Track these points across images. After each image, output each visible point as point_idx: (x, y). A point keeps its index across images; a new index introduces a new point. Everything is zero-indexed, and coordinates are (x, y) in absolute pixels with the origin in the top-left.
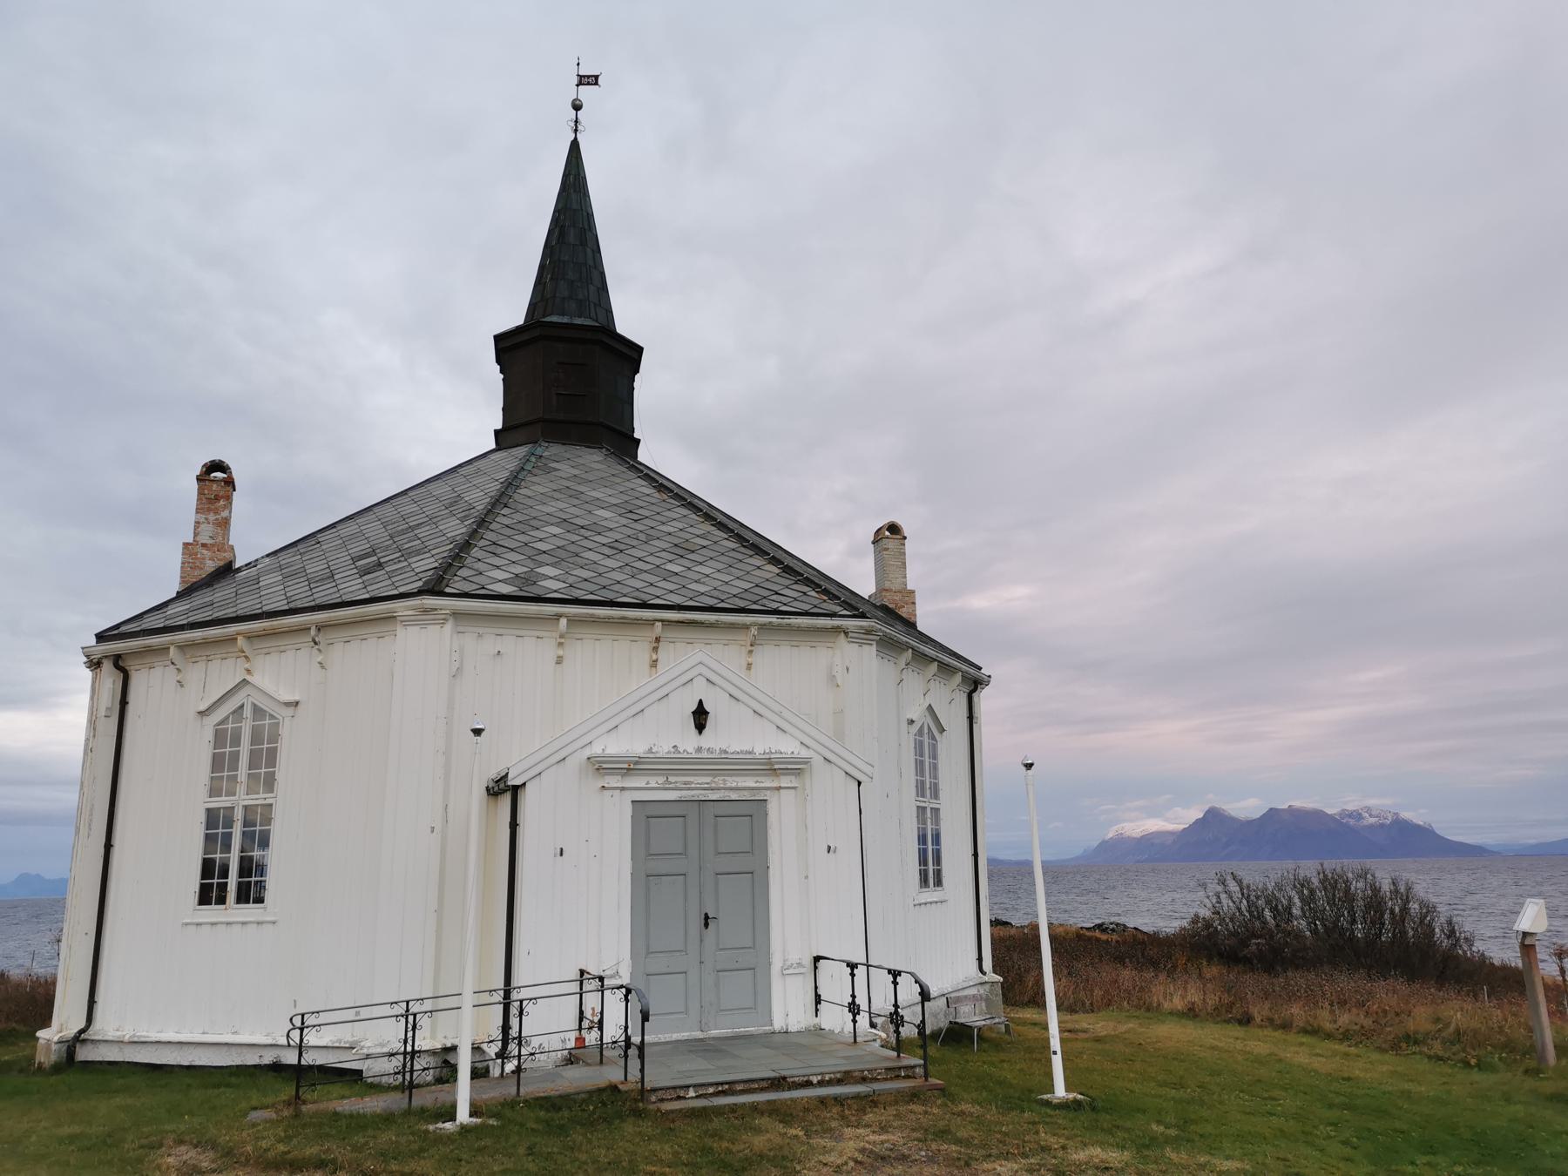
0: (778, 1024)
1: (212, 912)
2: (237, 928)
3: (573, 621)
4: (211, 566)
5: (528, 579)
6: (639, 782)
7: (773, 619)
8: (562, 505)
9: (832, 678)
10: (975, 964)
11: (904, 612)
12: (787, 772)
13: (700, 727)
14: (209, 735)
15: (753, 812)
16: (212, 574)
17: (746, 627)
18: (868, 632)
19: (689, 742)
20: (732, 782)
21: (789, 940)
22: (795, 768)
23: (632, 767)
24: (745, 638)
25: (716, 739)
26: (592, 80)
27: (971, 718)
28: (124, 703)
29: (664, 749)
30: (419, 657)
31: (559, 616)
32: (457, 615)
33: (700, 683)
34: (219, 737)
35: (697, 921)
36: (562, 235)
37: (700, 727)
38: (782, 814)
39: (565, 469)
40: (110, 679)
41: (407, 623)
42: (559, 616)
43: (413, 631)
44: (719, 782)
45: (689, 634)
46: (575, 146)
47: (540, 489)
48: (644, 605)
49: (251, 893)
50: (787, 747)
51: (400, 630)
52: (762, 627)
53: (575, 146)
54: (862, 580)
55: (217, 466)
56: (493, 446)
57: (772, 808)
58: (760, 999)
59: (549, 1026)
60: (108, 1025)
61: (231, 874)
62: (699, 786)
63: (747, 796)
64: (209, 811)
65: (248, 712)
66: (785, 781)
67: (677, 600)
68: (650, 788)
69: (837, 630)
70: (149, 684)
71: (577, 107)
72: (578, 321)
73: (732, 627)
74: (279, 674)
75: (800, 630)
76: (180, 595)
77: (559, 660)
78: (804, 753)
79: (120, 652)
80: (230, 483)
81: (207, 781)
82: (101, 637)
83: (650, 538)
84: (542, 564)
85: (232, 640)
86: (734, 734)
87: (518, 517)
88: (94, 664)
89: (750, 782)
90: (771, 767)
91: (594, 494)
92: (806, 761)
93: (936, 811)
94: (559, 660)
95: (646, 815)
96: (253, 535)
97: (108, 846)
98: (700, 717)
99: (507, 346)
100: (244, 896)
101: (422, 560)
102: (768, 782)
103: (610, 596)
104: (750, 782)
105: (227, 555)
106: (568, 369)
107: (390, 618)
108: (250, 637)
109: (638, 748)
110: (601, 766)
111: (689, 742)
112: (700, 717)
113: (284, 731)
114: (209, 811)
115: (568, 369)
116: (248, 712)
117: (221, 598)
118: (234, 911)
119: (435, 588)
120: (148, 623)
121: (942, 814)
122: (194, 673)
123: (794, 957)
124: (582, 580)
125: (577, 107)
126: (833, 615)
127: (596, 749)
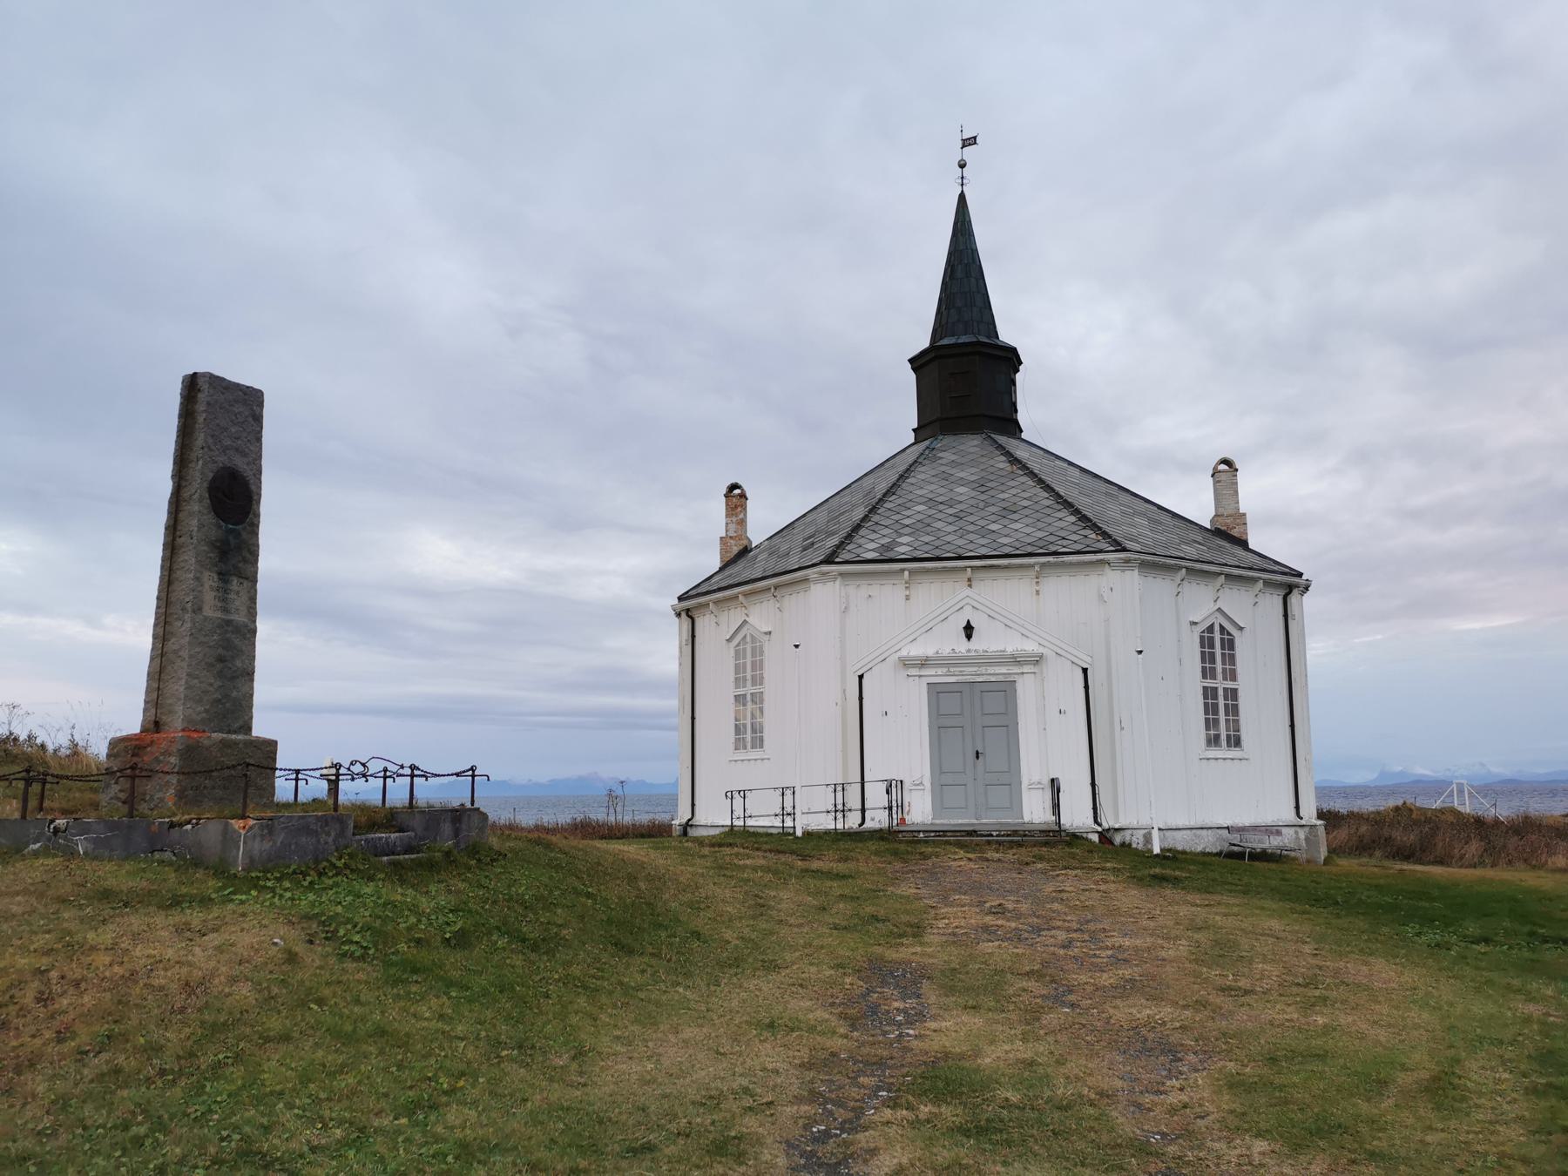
0: (1026, 819)
3: (911, 572)
4: (736, 550)
5: (887, 547)
6: (932, 672)
7: (1051, 559)
8: (933, 487)
9: (1101, 597)
10: (1293, 811)
11: (1235, 533)
12: (1027, 663)
13: (969, 637)
14: (732, 653)
15: (1007, 689)
16: (738, 554)
17: (1032, 566)
18: (1127, 561)
19: (962, 646)
20: (991, 670)
21: (1033, 770)
22: (1037, 660)
23: (924, 663)
24: (1032, 573)
25: (978, 644)
26: (969, 142)
27: (1286, 616)
28: (693, 636)
29: (946, 651)
30: (823, 601)
31: (903, 570)
32: (841, 574)
33: (968, 608)
34: (737, 652)
35: (972, 755)
36: (953, 271)
37: (969, 637)
38: (1026, 690)
39: (948, 456)
40: (686, 622)
41: (816, 581)
42: (903, 570)
43: (819, 586)
44: (983, 670)
45: (1018, 573)
46: (962, 197)
47: (922, 476)
48: (960, 558)
49: (758, 743)
50: (1030, 647)
52: (1043, 565)
53: (962, 197)
54: (1199, 506)
55: (734, 486)
57: (1019, 686)
58: (1016, 803)
60: (700, 819)
61: (749, 735)
62: (969, 674)
63: (1001, 678)
65: (748, 639)
66: (1026, 669)
67: (984, 551)
68: (938, 675)
69: (1101, 562)
70: (704, 623)
71: (962, 166)
72: (964, 339)
73: (1021, 566)
74: (761, 615)
75: (1071, 564)
76: (721, 569)
77: (907, 598)
78: (1041, 650)
79: (691, 605)
80: (743, 496)
81: (732, 679)
82: (680, 599)
83: (987, 505)
84: (901, 535)
85: (736, 597)
86: (989, 641)
87: (900, 501)
88: (679, 615)
89: (1004, 670)
90: (1016, 660)
91: (962, 475)
92: (1041, 656)
93: (1233, 694)
94: (907, 598)
95: (936, 691)
96: (762, 523)
97: (693, 718)
98: (969, 630)
101: (844, 539)
102: (1016, 670)
103: (937, 553)
104: (1004, 670)
105: (745, 542)
106: (967, 375)
107: (806, 580)
108: (746, 595)
109: (930, 652)
110: (906, 663)
111: (962, 646)
112: (969, 630)
113: (766, 649)
115: (967, 375)
116: (1217, 628)
117: (741, 571)
119: (829, 560)
120: (700, 590)
121: (1240, 693)
122: (724, 617)
123: (1036, 779)
124: (924, 543)
125: (962, 166)
126: (1101, 551)
127: (904, 653)
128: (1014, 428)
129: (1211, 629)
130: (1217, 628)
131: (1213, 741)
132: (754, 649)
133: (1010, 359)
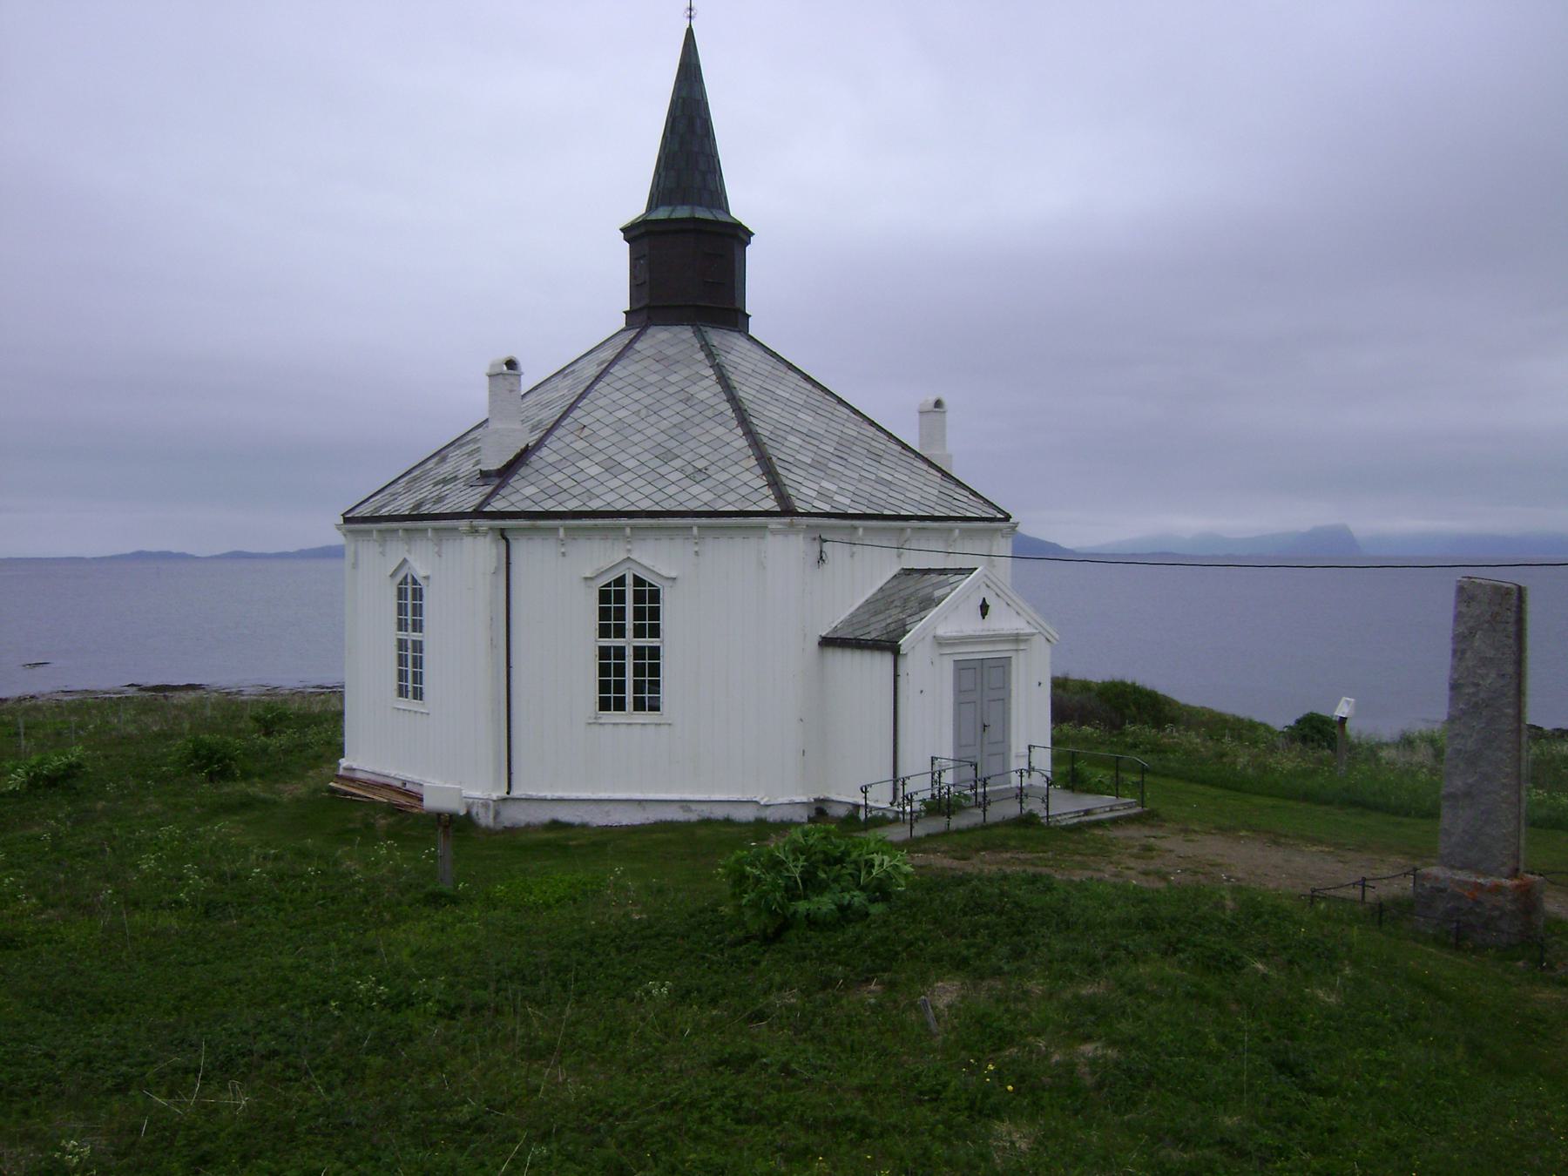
1: (613, 716)
2: (623, 728)
15: (1004, 664)
22: (405, 561)
35: (979, 729)
43: (779, 538)
46: (690, 33)
51: (769, 538)
53: (690, 33)
56: (1531, 718)
57: (1014, 661)
59: (920, 787)
64: (601, 648)
90: (1017, 639)
95: (961, 667)
98: (984, 609)
99: (635, 233)
100: (639, 705)
106: (688, 258)
112: (984, 609)
114: (601, 648)
115: (688, 258)
116: (629, 581)
118: (629, 715)
128: (733, 317)
129: (620, 581)
130: (629, 581)
131: (604, 705)
132: (414, 590)
133: (739, 235)
